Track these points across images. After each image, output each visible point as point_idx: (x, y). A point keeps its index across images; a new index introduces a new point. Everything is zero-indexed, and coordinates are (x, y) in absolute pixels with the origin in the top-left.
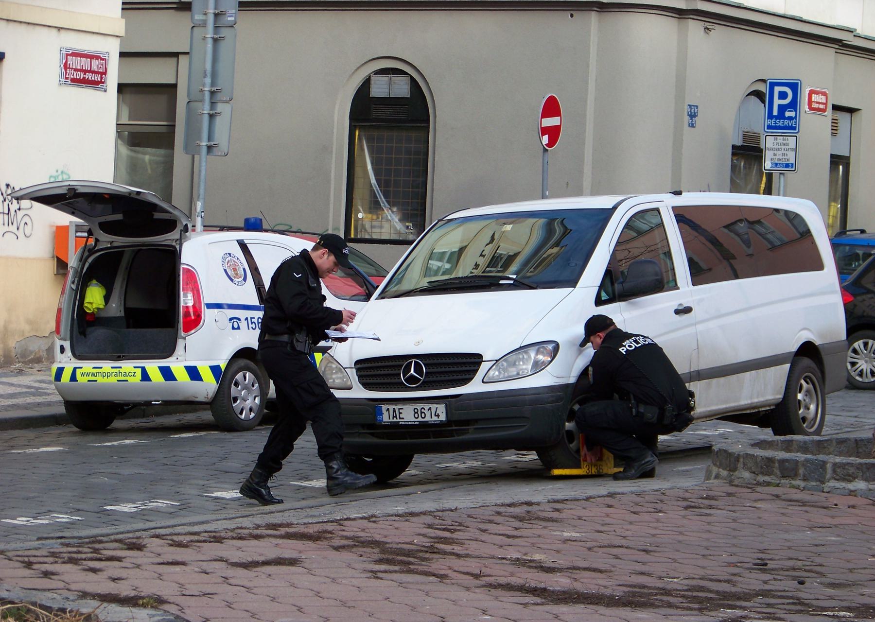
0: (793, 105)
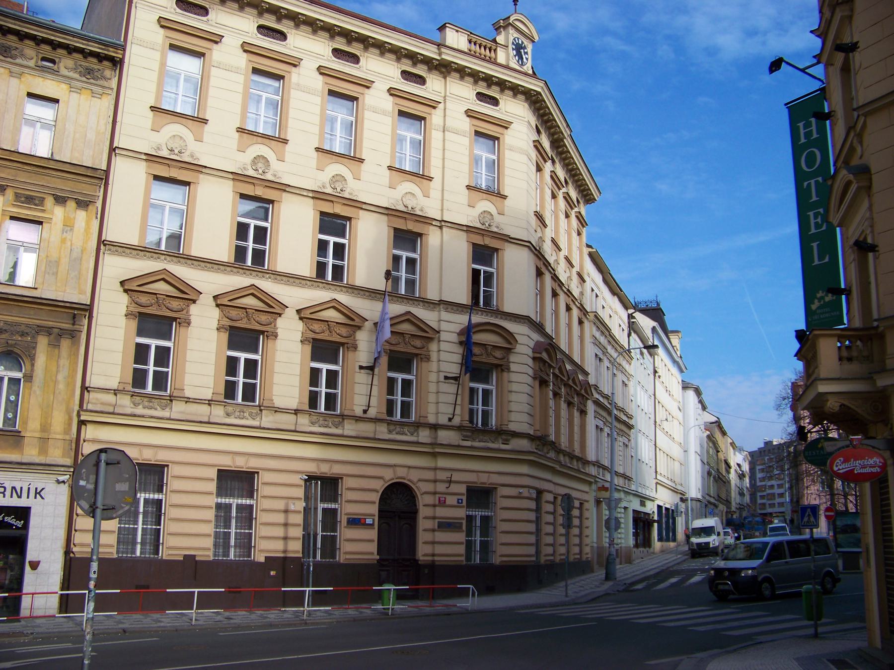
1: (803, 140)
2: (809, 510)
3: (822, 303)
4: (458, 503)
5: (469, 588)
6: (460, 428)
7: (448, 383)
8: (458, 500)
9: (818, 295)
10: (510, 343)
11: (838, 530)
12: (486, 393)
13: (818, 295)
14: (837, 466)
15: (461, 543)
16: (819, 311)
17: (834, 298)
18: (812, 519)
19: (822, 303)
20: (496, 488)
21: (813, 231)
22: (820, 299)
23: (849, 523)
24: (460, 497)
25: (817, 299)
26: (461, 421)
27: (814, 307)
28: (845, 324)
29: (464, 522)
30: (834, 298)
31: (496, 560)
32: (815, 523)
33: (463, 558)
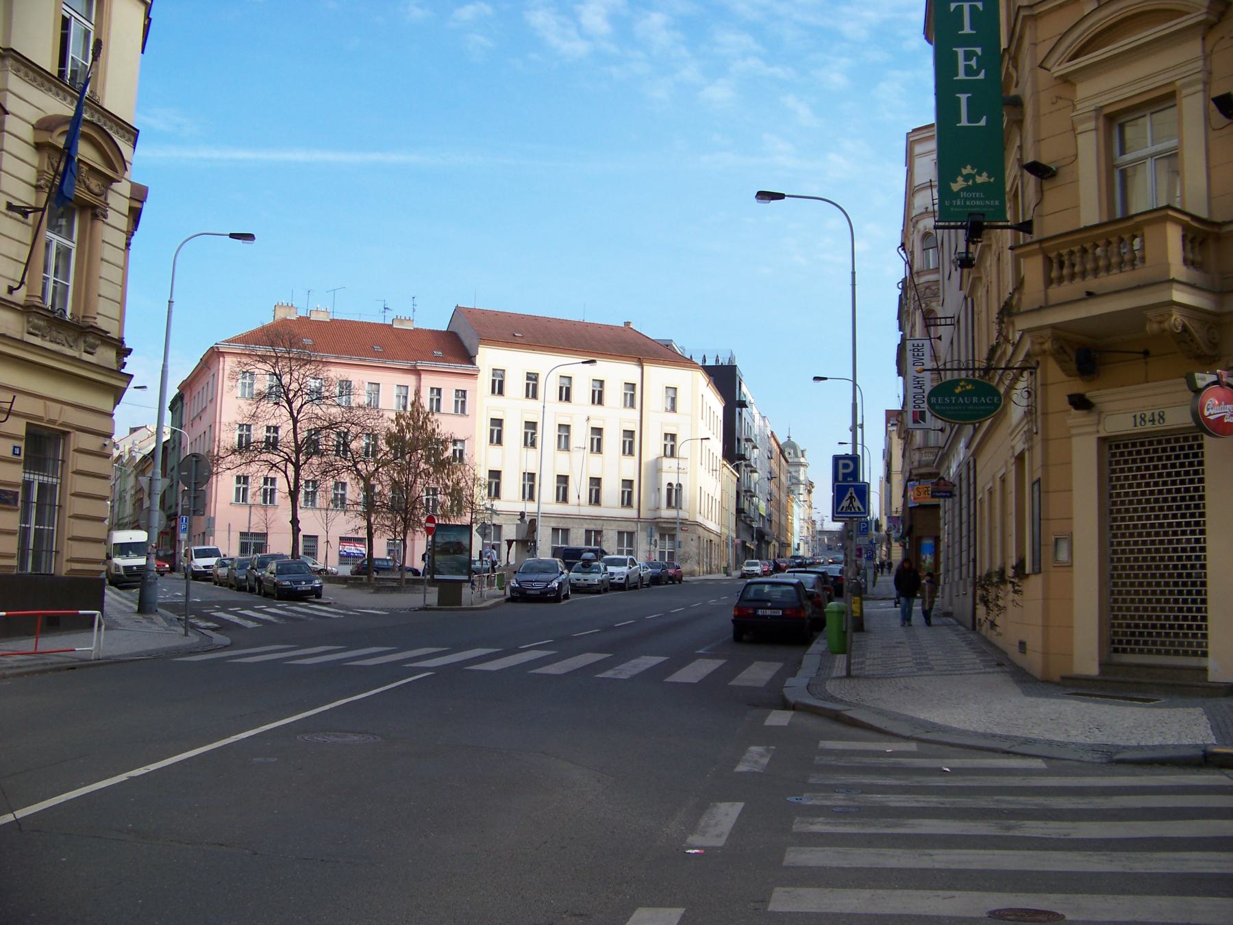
0: (867, 528)
3: (970, 183)
4: (14, 453)
5: (94, 615)
6: (27, 310)
7: (11, 217)
8: (15, 447)
9: (964, 172)
10: (115, 171)
11: (437, 549)
12: (64, 254)
13: (964, 172)
14: (1208, 409)
15: (10, 533)
17: (992, 180)
18: (857, 503)
19: (970, 183)
20: (66, 434)
21: (961, 75)
22: (967, 178)
23: (452, 539)
24: (17, 443)
25: (963, 176)
26: (27, 296)
27: (955, 187)
28: (1008, 221)
29: (20, 490)
30: (992, 180)
31: (63, 568)
32: (862, 510)
33: (14, 562)
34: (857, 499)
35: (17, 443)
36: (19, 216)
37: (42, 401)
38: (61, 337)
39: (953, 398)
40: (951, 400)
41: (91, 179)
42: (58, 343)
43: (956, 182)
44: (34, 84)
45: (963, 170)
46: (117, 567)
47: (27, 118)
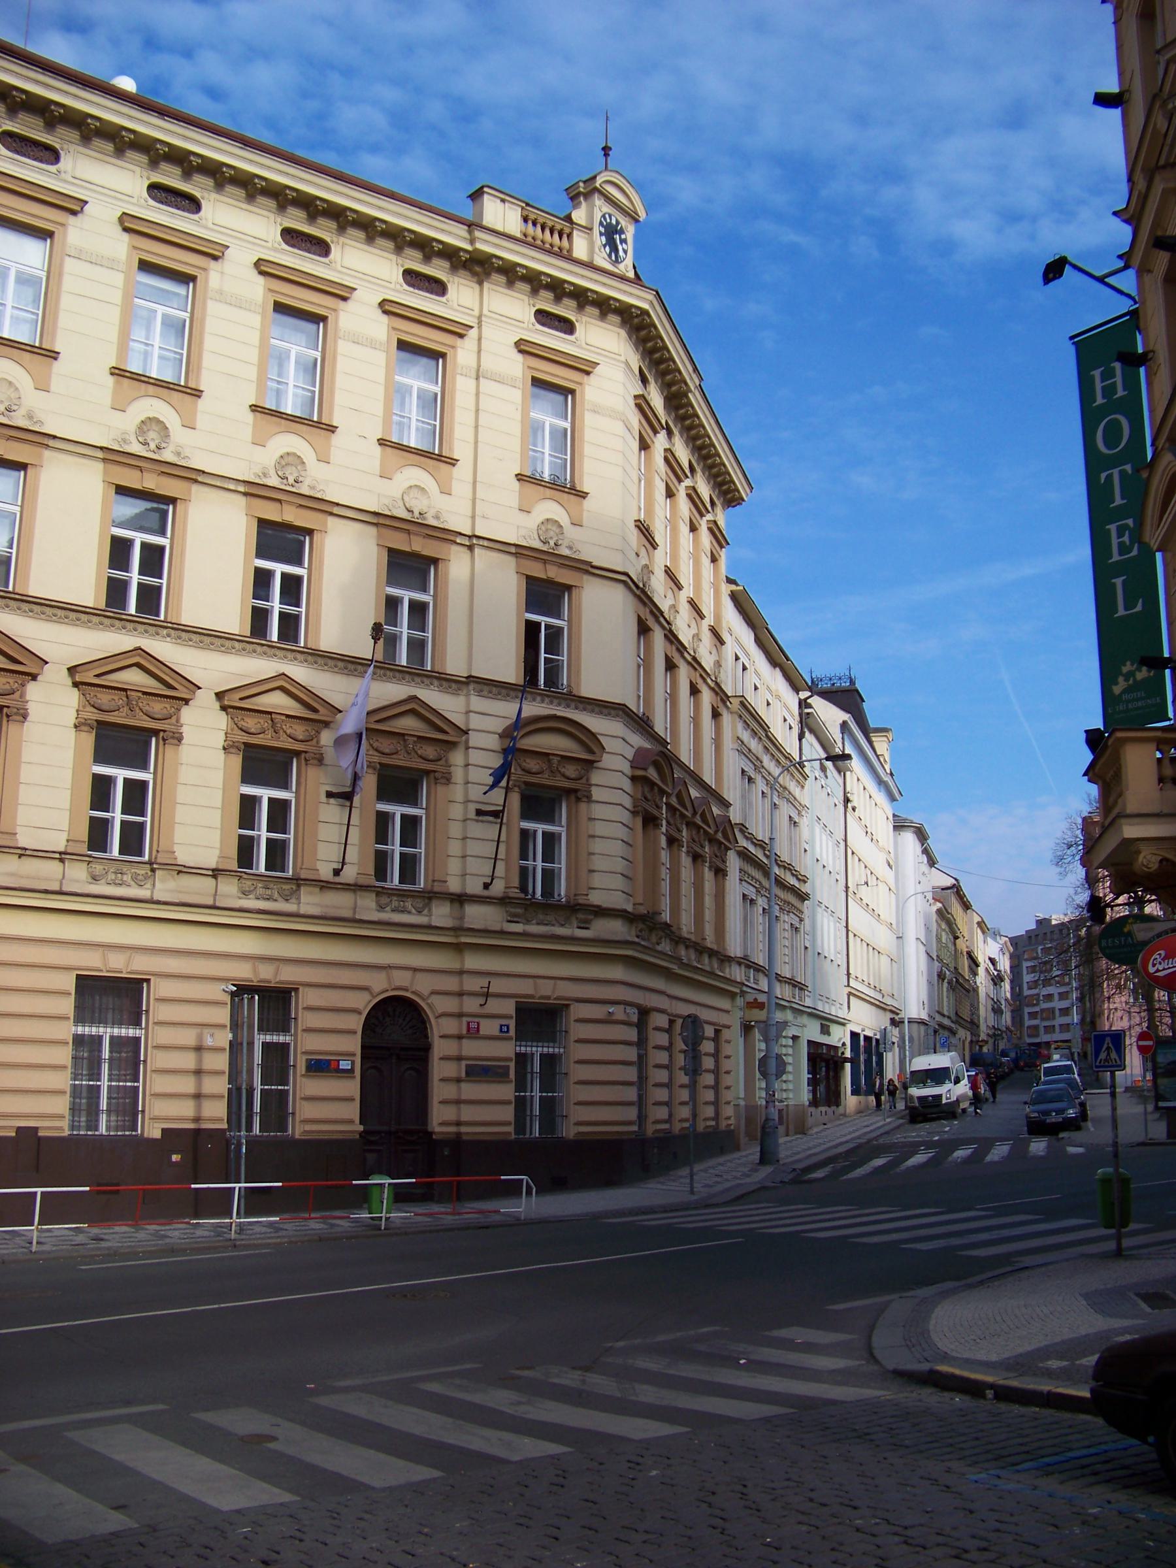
1: (1100, 400)
2: (1108, 1040)
3: (1131, 682)
5: (523, 1180)
7: (482, 821)
8: (501, 1026)
9: (1125, 669)
11: (1159, 1071)
13: (1125, 669)
15: (506, 1102)
16: (1124, 697)
18: (1114, 1055)
19: (1131, 682)
20: (567, 1006)
21: (1116, 557)
25: (1123, 675)
26: (506, 888)
27: (1117, 690)
28: (1170, 720)
29: (512, 1065)
31: (569, 1131)
32: (1119, 1063)
33: (511, 1129)
34: (1114, 1052)
35: (504, 1022)
36: (491, 819)
37: (531, 980)
38: (550, 918)
39: (1123, 939)
40: (1120, 942)
41: (567, 766)
42: (547, 925)
43: (1117, 684)
44: (499, 697)
45: (1123, 668)
46: (912, 1097)
47: (492, 730)
